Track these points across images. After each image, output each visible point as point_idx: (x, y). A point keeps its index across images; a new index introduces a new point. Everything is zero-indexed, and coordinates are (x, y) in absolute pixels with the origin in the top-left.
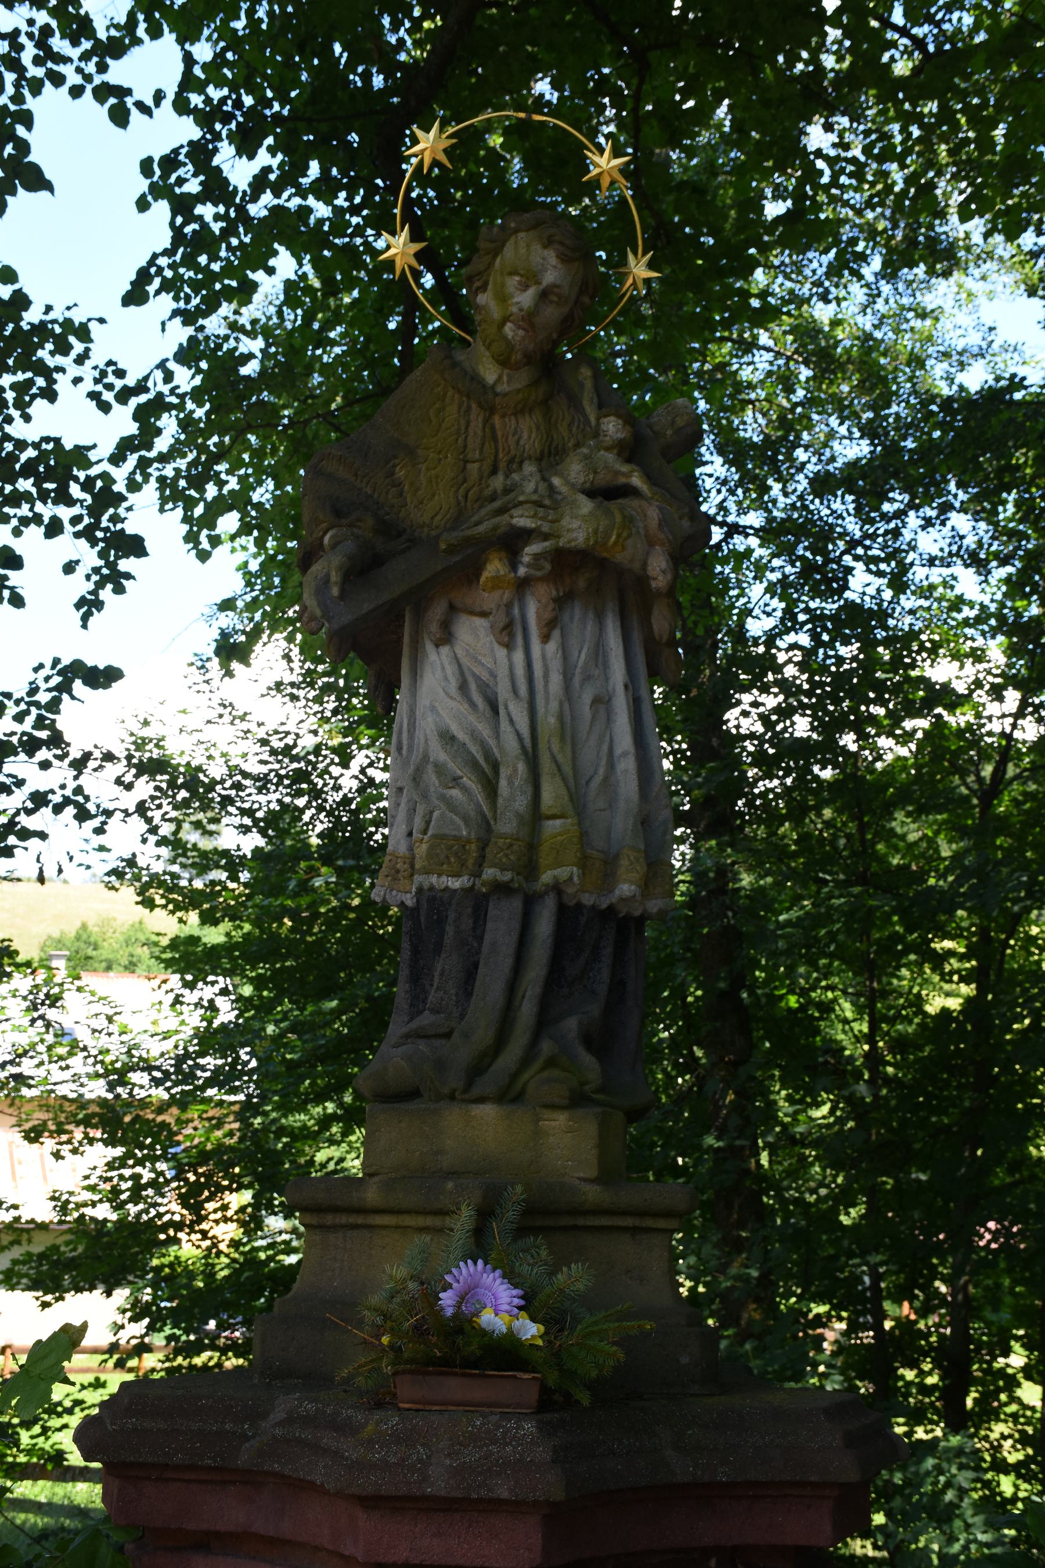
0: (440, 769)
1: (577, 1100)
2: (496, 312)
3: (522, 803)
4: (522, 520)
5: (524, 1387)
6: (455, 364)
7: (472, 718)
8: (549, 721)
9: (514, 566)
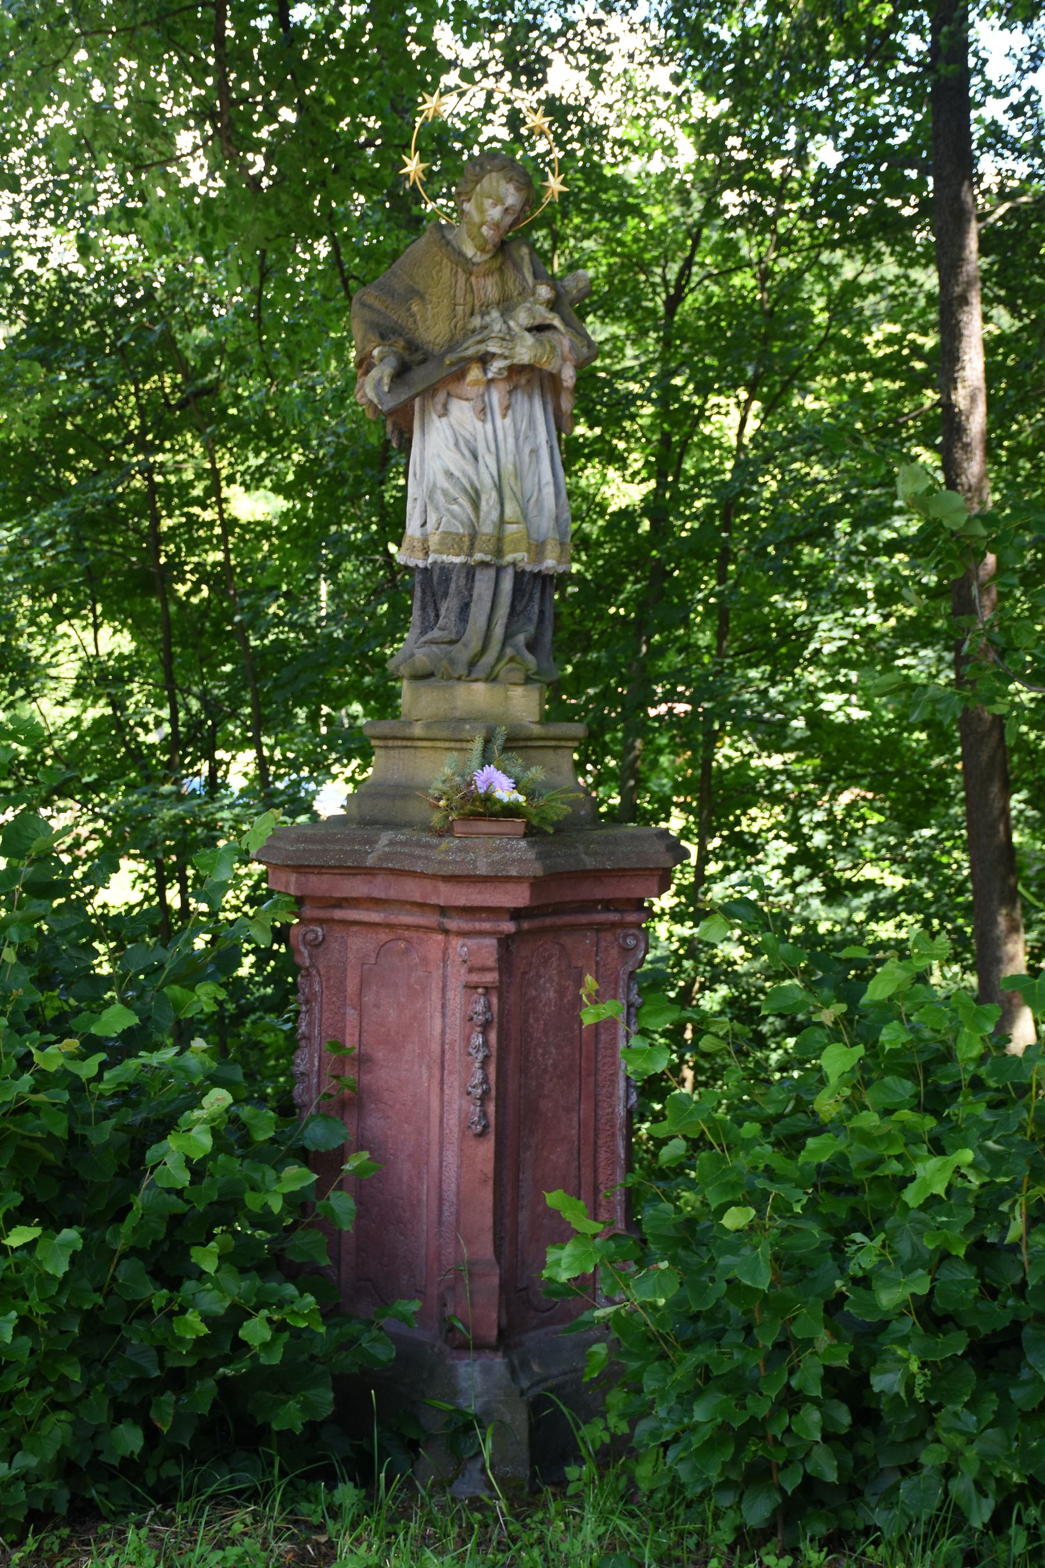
0: (445, 493)
1: (528, 680)
2: (476, 218)
3: (495, 515)
4: (493, 348)
5: (518, 825)
6: (448, 243)
7: (462, 462)
8: (508, 467)
9: (485, 371)
